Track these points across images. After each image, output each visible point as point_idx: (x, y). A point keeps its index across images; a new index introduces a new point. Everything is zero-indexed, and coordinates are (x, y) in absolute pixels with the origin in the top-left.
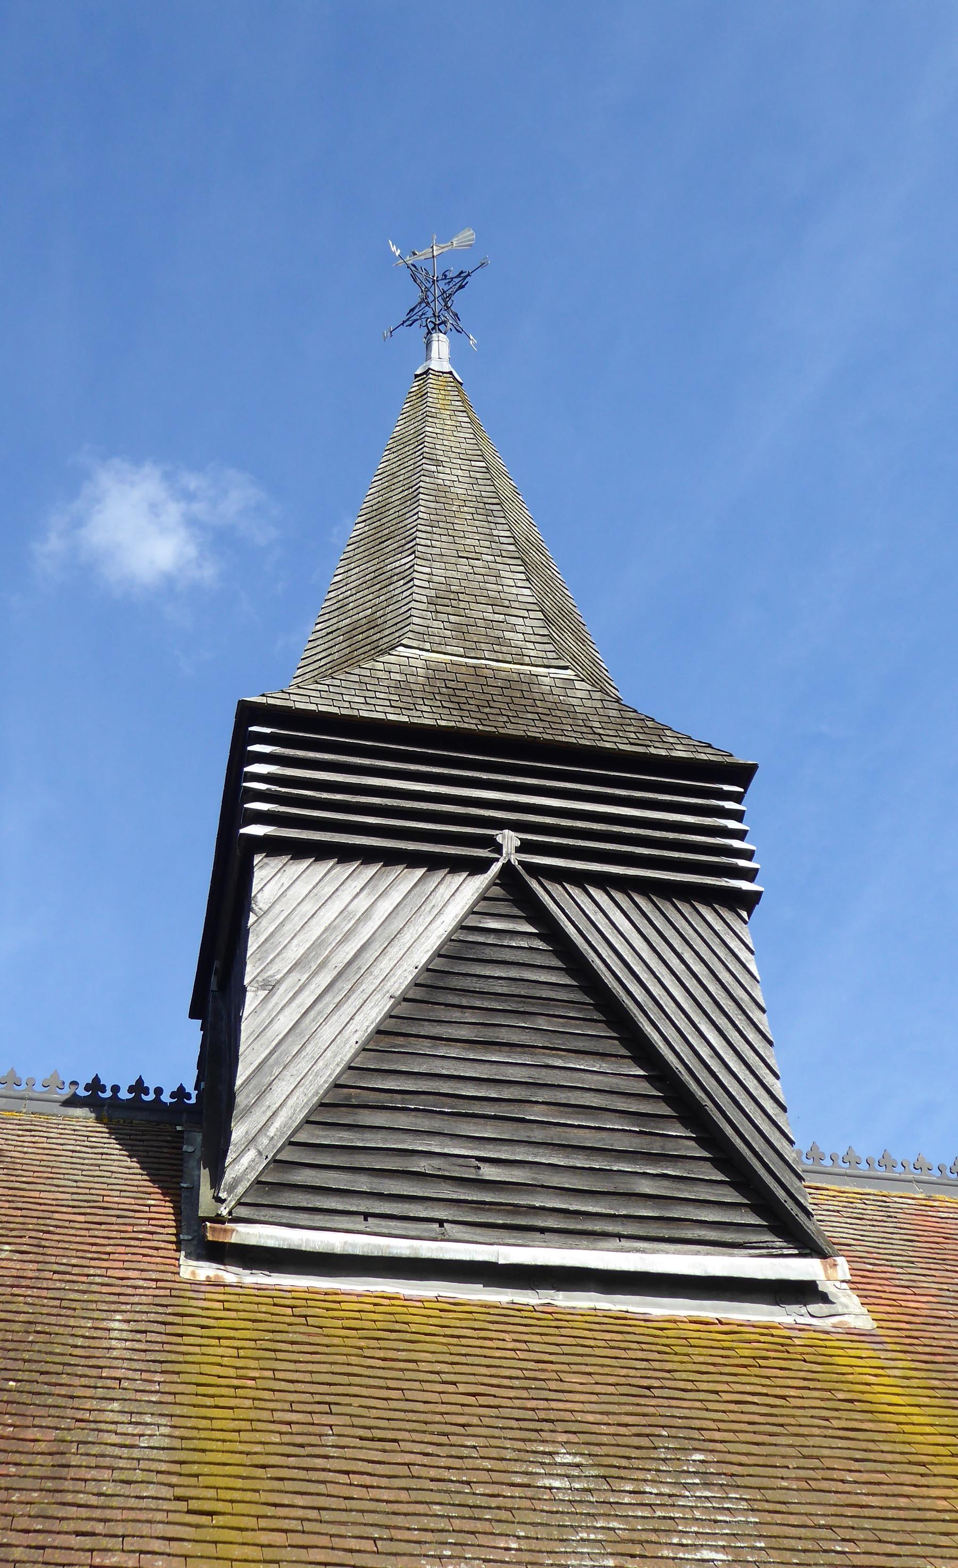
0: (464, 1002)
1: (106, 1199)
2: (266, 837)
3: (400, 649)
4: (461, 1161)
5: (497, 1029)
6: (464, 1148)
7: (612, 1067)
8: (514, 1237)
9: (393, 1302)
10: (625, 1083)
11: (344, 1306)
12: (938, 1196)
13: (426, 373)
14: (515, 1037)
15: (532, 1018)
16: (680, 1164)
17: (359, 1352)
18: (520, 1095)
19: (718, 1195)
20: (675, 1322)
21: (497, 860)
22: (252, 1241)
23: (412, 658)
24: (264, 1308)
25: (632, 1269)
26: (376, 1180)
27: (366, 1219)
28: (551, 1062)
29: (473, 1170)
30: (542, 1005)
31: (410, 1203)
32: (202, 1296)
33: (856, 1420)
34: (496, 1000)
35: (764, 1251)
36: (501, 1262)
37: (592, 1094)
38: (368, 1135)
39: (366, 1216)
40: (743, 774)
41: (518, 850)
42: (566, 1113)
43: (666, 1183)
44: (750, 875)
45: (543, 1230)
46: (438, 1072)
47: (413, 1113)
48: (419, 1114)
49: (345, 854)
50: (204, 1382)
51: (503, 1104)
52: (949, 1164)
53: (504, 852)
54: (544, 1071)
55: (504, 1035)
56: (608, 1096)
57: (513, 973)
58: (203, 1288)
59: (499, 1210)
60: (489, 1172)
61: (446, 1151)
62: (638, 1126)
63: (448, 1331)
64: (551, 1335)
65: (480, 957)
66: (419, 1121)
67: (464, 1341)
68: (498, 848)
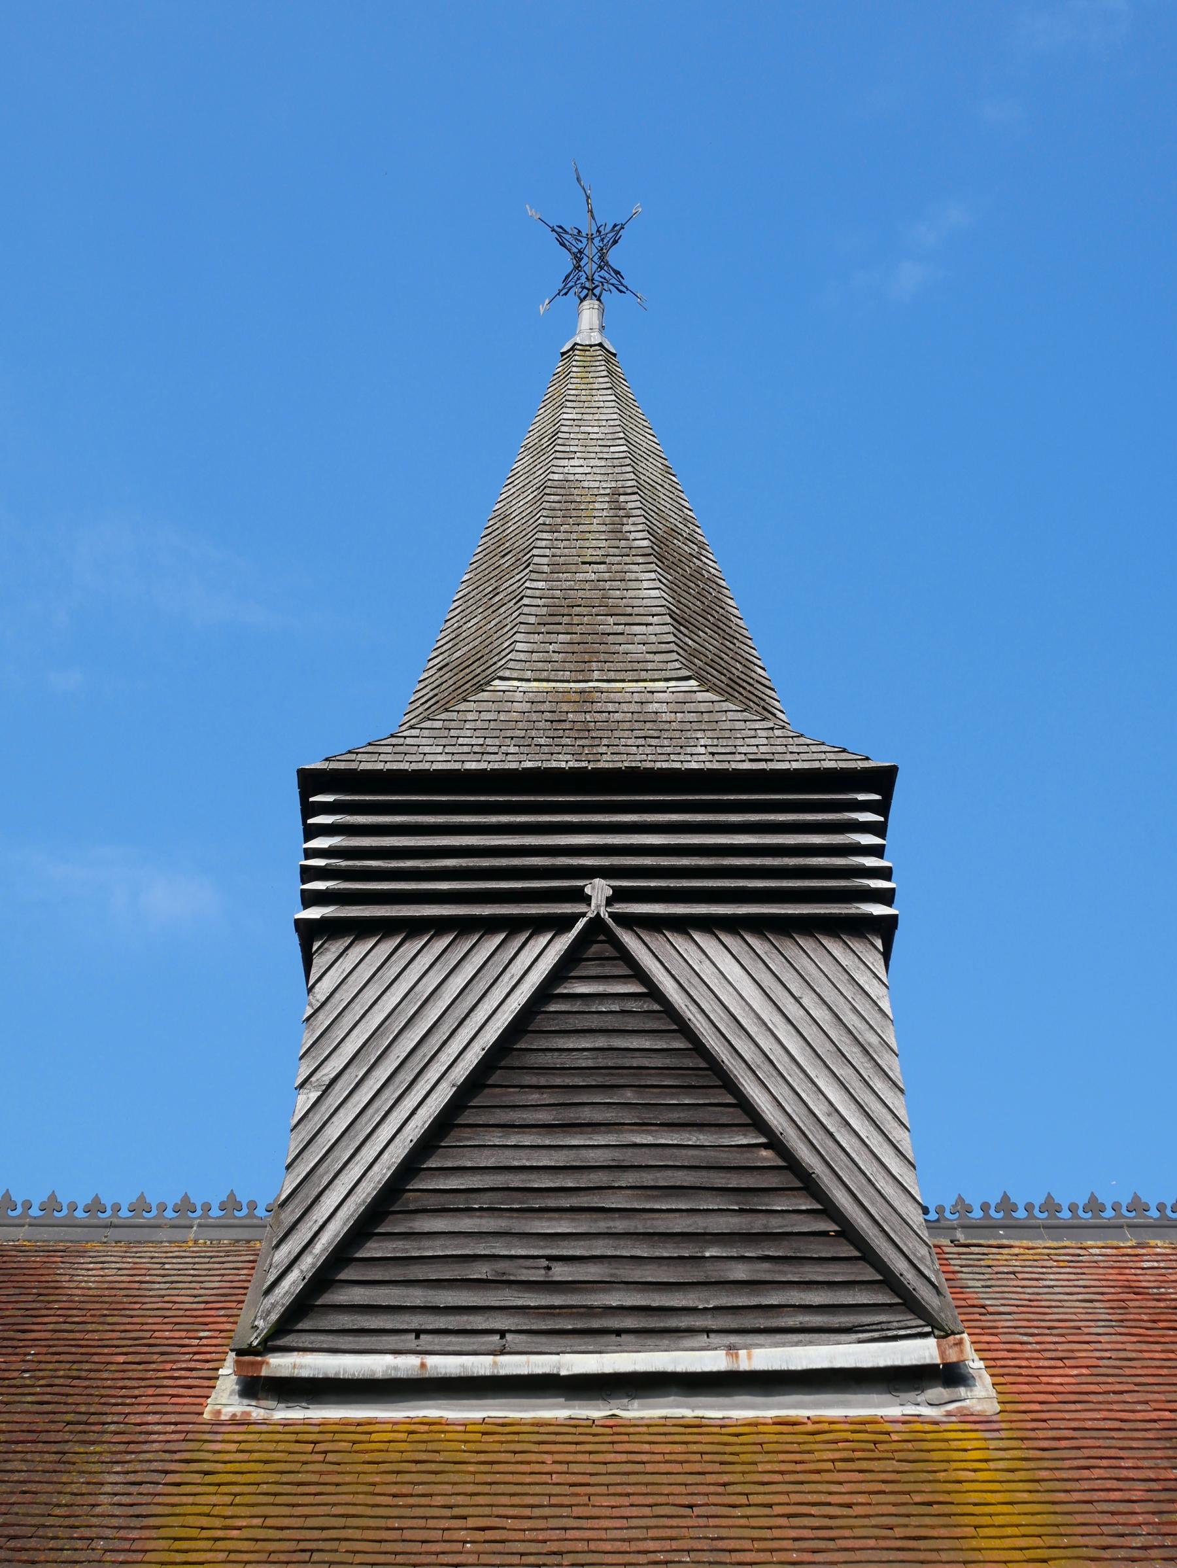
0: (543, 1081)
1: (156, 1334)
2: (323, 920)
3: (497, 682)
4: (530, 1263)
5: (580, 1109)
6: (534, 1247)
7: (711, 1138)
8: (585, 1344)
9: (433, 1428)
10: (724, 1155)
11: (374, 1437)
12: (1152, 1243)
13: (572, 349)
14: (609, 1115)
15: (620, 1091)
16: (785, 1243)
17: (371, 1489)
18: (601, 1181)
19: (828, 1274)
20: (756, 1425)
21: (584, 915)
22: (285, 1373)
23: (517, 690)
24: (282, 1446)
25: (699, 1370)
26: (431, 1292)
27: (417, 1337)
28: (639, 1140)
29: (543, 1272)
30: (635, 1075)
31: (470, 1314)
32: (219, 1437)
33: (926, 1526)
34: (579, 1075)
35: (876, 1335)
36: (563, 1373)
37: (685, 1172)
38: (426, 1243)
39: (418, 1333)
40: (882, 780)
41: (609, 901)
42: (657, 1196)
43: (766, 1266)
44: (886, 897)
45: (619, 1332)
46: (508, 1164)
47: (478, 1214)
48: (484, 1214)
49: (412, 928)
50: (183, 1535)
51: (582, 1193)
52: (1169, 1203)
53: (593, 904)
54: (630, 1152)
55: (587, 1115)
56: (704, 1173)
57: (601, 1042)
58: (224, 1429)
59: (571, 1314)
60: (560, 1272)
61: (513, 1253)
62: (737, 1204)
63: (483, 1457)
64: (602, 1452)
65: (563, 1027)
66: (484, 1221)
67: (496, 1468)
68: (587, 900)
